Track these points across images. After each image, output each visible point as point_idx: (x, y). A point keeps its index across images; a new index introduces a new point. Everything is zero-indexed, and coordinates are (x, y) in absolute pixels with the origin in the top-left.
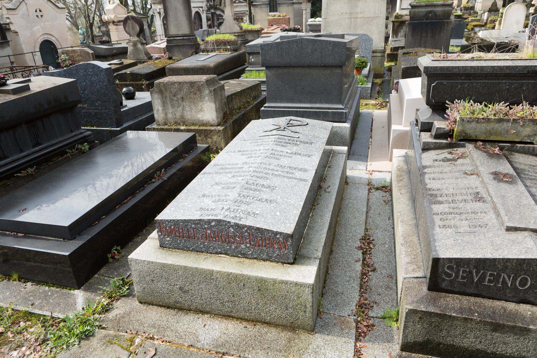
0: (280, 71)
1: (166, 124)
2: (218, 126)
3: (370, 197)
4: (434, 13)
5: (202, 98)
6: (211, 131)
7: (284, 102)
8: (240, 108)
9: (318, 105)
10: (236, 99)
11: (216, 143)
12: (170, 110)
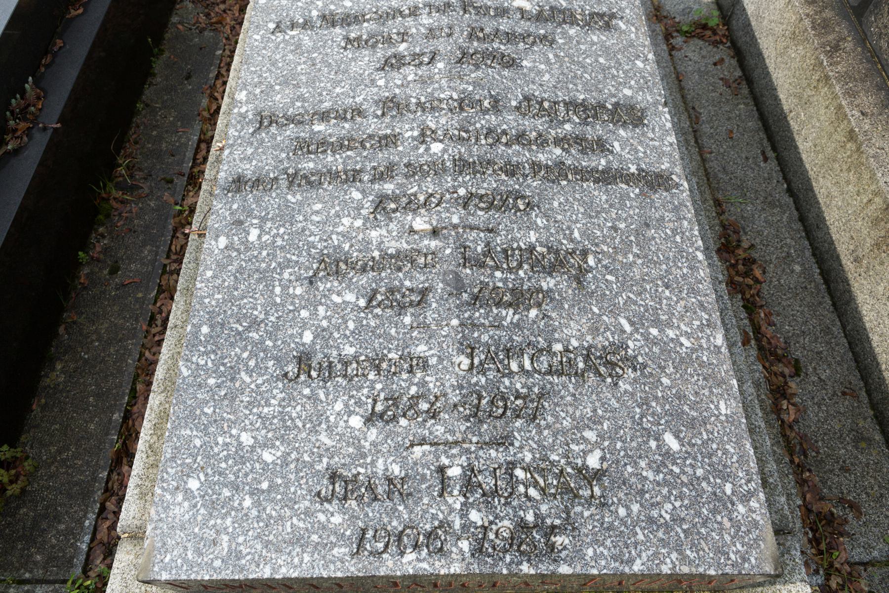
3: (681, 69)
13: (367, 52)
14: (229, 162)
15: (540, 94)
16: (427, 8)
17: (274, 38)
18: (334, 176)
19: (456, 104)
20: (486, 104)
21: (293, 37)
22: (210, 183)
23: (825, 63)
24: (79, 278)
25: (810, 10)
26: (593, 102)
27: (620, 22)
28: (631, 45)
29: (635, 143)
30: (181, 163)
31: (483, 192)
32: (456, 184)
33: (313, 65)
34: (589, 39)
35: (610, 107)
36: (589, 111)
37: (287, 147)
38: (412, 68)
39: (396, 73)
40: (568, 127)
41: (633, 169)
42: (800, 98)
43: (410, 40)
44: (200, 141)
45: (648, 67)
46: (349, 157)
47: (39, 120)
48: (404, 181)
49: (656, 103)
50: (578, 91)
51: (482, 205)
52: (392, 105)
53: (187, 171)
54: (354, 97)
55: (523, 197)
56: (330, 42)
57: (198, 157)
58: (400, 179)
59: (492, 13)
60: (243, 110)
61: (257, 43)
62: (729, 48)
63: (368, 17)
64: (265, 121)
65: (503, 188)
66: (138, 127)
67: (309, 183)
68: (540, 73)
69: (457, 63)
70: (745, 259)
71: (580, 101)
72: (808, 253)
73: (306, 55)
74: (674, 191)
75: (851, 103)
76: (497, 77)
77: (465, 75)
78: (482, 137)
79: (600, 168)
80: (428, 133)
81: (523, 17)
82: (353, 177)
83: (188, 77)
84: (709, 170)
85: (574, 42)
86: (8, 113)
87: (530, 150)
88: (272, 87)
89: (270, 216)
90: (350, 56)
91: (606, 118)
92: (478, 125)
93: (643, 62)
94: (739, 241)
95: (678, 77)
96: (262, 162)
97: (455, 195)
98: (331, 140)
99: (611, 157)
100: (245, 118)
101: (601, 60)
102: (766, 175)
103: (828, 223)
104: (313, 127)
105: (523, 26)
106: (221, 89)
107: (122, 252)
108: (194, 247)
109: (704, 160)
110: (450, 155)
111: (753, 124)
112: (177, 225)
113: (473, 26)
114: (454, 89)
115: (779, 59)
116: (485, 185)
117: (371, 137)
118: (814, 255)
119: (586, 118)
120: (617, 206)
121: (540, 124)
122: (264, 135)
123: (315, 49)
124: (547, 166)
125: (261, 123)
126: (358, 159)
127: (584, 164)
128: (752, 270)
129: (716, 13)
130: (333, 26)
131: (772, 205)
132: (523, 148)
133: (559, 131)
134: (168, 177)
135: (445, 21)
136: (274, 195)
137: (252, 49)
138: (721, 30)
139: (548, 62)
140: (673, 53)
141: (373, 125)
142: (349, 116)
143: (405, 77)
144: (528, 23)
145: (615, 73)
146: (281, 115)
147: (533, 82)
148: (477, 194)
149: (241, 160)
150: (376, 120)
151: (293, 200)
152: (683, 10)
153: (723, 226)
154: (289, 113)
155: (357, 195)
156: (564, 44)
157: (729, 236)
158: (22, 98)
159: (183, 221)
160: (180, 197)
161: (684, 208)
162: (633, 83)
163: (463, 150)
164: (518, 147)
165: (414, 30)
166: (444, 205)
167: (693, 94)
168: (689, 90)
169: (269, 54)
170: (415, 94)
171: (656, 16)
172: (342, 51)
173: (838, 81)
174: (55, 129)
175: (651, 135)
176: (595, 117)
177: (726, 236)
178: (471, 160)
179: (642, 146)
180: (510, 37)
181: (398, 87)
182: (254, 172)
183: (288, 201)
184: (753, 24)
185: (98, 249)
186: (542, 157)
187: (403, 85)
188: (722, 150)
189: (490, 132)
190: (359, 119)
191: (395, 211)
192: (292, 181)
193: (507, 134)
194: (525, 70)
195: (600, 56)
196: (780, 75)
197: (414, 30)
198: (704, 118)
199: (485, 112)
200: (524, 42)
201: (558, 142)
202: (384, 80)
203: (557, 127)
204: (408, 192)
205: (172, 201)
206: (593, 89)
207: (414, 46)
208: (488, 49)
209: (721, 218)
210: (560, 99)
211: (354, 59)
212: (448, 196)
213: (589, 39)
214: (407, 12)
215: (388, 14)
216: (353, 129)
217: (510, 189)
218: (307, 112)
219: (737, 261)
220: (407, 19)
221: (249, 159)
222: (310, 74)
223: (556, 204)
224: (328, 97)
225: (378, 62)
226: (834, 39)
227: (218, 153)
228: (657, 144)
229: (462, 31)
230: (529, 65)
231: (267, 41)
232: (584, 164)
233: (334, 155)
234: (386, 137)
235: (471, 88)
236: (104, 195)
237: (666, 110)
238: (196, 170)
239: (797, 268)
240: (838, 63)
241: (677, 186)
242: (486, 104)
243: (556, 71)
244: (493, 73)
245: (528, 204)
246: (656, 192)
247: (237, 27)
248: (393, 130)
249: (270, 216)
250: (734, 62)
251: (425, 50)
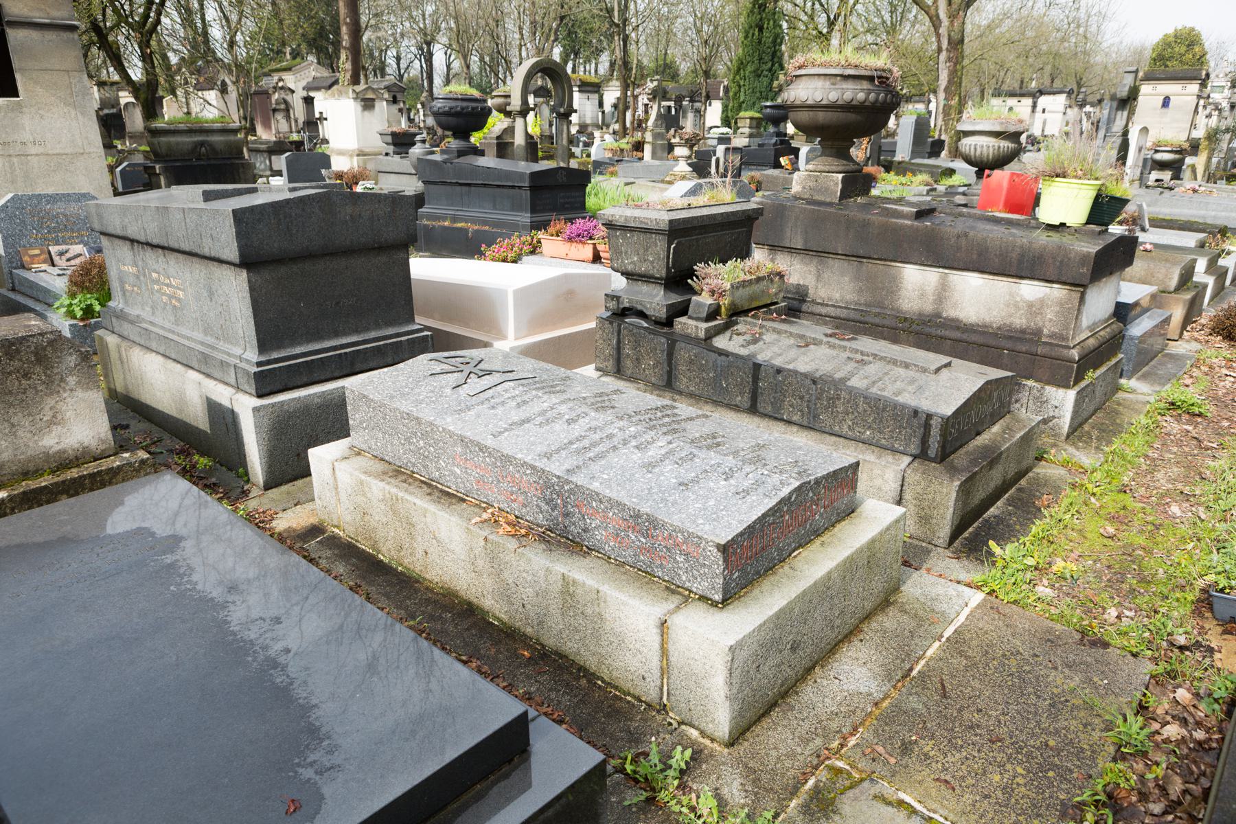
0: (283, 270)
4: (210, 144)
5: (53, 384)
7: (300, 344)
9: (373, 334)
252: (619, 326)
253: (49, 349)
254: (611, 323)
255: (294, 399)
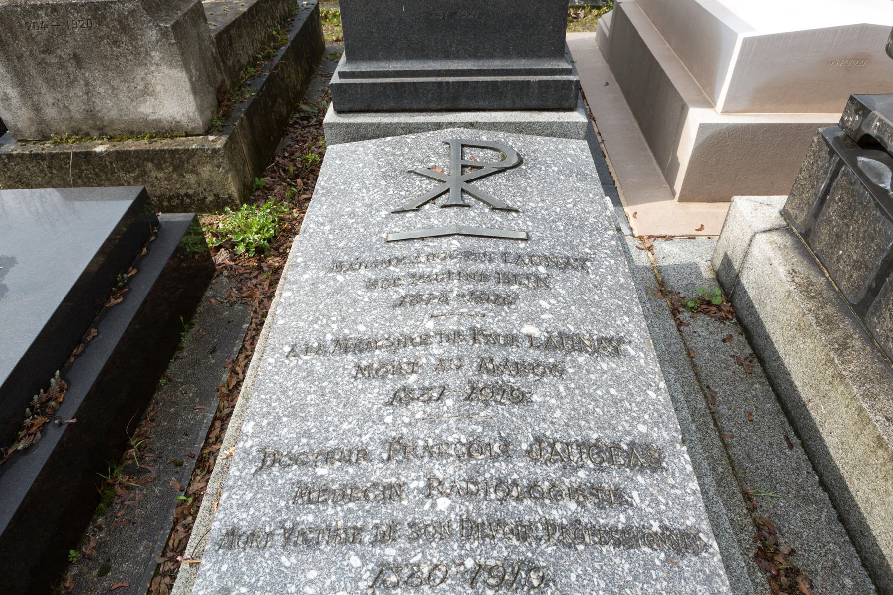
1: (45, 138)
2: (208, 132)
3: (691, 345)
5: (140, 56)
6: (191, 153)
7: (398, 59)
8: (256, 59)
9: (497, 64)
10: (240, 37)
11: (210, 183)
12: (48, 97)
13: (377, 383)
14: (225, 509)
15: (552, 434)
16: (438, 337)
17: (287, 362)
18: (333, 533)
19: (464, 450)
20: (496, 448)
21: (306, 362)
22: (211, 499)
23: (837, 362)
24: (65, 580)
25: (811, 305)
26: (608, 441)
27: (628, 347)
28: (642, 373)
29: (655, 492)
30: (192, 444)
31: (491, 563)
32: (463, 552)
33: (323, 395)
34: (598, 368)
35: (625, 447)
36: (604, 453)
37: (287, 493)
38: (421, 404)
39: (404, 410)
40: (582, 474)
41: (656, 527)
42: (817, 390)
43: (420, 371)
44: (215, 419)
45: (660, 398)
46: (350, 510)
47: (58, 414)
48: (408, 545)
49: (673, 441)
50: (591, 429)
51: (492, 581)
52: (398, 447)
53: (197, 453)
54: (360, 436)
55: (537, 569)
56: (341, 369)
57: (211, 436)
58: (403, 543)
59: (502, 342)
60: (248, 445)
61: (271, 368)
62: (735, 324)
63: (380, 343)
64: (269, 459)
65: (514, 557)
66: (157, 403)
67: (306, 541)
68: (550, 409)
69: (466, 399)
70: (787, 569)
71: (593, 442)
72: (857, 563)
73: (316, 383)
74: (704, 554)
75: (873, 406)
76: (507, 415)
77: (474, 414)
78: (492, 490)
79: (620, 526)
80: (435, 484)
81: (532, 345)
82: (353, 536)
83: (213, 351)
84: (733, 458)
85: (584, 371)
86: (28, 409)
87: (543, 505)
88: (280, 418)
89: (260, 584)
90: (360, 387)
91: (622, 462)
92: (487, 475)
93: (655, 392)
94: (777, 544)
95: (689, 354)
96: (260, 511)
97: (462, 568)
98: (334, 488)
99: (630, 511)
100: (248, 454)
101: (613, 391)
102: (794, 464)
103: (874, 533)
104: (316, 470)
105: (533, 355)
106: (243, 364)
107: (117, 548)
108: (183, 580)
109: (726, 446)
110: (457, 514)
111: (771, 405)
112: (178, 516)
113: (483, 356)
114: (461, 431)
115: (788, 346)
116: (495, 554)
117: (375, 485)
118: (864, 565)
119: (601, 463)
120: (642, 577)
121: (553, 471)
122: (265, 476)
123: (326, 377)
124: (562, 526)
125: (264, 461)
126: (360, 513)
127: (602, 521)
128: (797, 583)
129: (718, 291)
130: (346, 352)
131: (806, 500)
132: (535, 503)
133: (573, 479)
134: (178, 460)
135: (455, 351)
136: (267, 555)
137: (265, 374)
138: (725, 306)
139: (558, 396)
140: (681, 328)
141: (378, 472)
142: (354, 459)
143: (413, 415)
144: (537, 352)
145: (628, 405)
146: (285, 453)
147: (544, 420)
148: (486, 566)
149: (239, 506)
150: (381, 465)
151: (287, 564)
152: (687, 285)
153: (759, 527)
154: (293, 451)
155: (355, 561)
156: (574, 374)
157: (765, 539)
158: (45, 392)
159: (185, 512)
160: (187, 482)
161: (718, 579)
162: (647, 417)
163: (471, 508)
164: (529, 502)
165: (424, 361)
166: (449, 581)
167: (706, 371)
168: (701, 367)
169: (281, 381)
170: (423, 436)
171: (661, 291)
172: (352, 380)
173: (854, 381)
174: (70, 425)
175: (671, 481)
176: (611, 460)
177: (760, 537)
178: (480, 520)
179: (663, 495)
180: (520, 368)
181: (406, 425)
182: (250, 524)
183: (281, 564)
184: (756, 307)
185: (92, 544)
186: (556, 515)
187: (410, 424)
188: (743, 435)
189: (500, 482)
190: (364, 463)
191: (396, 585)
192: (288, 538)
193: (517, 486)
194: (536, 406)
195: (611, 386)
196: (791, 362)
197: (424, 361)
198: (720, 398)
199: (495, 458)
200: (533, 373)
201: (573, 493)
202: (392, 416)
203: (571, 474)
204: (411, 561)
205: (178, 486)
206: (606, 425)
207: (424, 379)
208: (497, 383)
209: (754, 514)
210: (573, 440)
211: (363, 391)
212: (454, 569)
213: (598, 368)
214: (418, 340)
215: (399, 341)
216: (357, 475)
217: (522, 558)
218: (312, 450)
219: (778, 571)
220: (418, 348)
221: (245, 506)
222: (318, 405)
223: (573, 577)
224: (335, 434)
225: (387, 395)
226: (841, 336)
227: (224, 461)
228: (678, 492)
229: (472, 363)
230: (539, 400)
231: (281, 366)
232: (602, 521)
233: (334, 507)
234: (391, 487)
235: (480, 430)
236: (110, 481)
237: (684, 448)
238: (207, 451)
239: (848, 582)
240: (850, 362)
241: (707, 547)
242: (496, 448)
243: (567, 406)
244: (504, 412)
245: (543, 578)
246: (683, 556)
247: (266, 300)
248: (398, 478)
249: (260, 584)
250: (742, 339)
251: (435, 384)
252: (841, 164)
253: (130, 19)
254: (832, 153)
255: (372, 125)
